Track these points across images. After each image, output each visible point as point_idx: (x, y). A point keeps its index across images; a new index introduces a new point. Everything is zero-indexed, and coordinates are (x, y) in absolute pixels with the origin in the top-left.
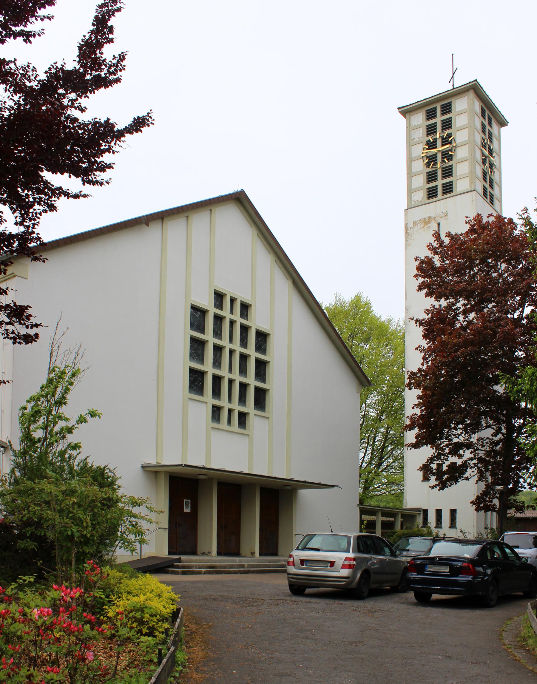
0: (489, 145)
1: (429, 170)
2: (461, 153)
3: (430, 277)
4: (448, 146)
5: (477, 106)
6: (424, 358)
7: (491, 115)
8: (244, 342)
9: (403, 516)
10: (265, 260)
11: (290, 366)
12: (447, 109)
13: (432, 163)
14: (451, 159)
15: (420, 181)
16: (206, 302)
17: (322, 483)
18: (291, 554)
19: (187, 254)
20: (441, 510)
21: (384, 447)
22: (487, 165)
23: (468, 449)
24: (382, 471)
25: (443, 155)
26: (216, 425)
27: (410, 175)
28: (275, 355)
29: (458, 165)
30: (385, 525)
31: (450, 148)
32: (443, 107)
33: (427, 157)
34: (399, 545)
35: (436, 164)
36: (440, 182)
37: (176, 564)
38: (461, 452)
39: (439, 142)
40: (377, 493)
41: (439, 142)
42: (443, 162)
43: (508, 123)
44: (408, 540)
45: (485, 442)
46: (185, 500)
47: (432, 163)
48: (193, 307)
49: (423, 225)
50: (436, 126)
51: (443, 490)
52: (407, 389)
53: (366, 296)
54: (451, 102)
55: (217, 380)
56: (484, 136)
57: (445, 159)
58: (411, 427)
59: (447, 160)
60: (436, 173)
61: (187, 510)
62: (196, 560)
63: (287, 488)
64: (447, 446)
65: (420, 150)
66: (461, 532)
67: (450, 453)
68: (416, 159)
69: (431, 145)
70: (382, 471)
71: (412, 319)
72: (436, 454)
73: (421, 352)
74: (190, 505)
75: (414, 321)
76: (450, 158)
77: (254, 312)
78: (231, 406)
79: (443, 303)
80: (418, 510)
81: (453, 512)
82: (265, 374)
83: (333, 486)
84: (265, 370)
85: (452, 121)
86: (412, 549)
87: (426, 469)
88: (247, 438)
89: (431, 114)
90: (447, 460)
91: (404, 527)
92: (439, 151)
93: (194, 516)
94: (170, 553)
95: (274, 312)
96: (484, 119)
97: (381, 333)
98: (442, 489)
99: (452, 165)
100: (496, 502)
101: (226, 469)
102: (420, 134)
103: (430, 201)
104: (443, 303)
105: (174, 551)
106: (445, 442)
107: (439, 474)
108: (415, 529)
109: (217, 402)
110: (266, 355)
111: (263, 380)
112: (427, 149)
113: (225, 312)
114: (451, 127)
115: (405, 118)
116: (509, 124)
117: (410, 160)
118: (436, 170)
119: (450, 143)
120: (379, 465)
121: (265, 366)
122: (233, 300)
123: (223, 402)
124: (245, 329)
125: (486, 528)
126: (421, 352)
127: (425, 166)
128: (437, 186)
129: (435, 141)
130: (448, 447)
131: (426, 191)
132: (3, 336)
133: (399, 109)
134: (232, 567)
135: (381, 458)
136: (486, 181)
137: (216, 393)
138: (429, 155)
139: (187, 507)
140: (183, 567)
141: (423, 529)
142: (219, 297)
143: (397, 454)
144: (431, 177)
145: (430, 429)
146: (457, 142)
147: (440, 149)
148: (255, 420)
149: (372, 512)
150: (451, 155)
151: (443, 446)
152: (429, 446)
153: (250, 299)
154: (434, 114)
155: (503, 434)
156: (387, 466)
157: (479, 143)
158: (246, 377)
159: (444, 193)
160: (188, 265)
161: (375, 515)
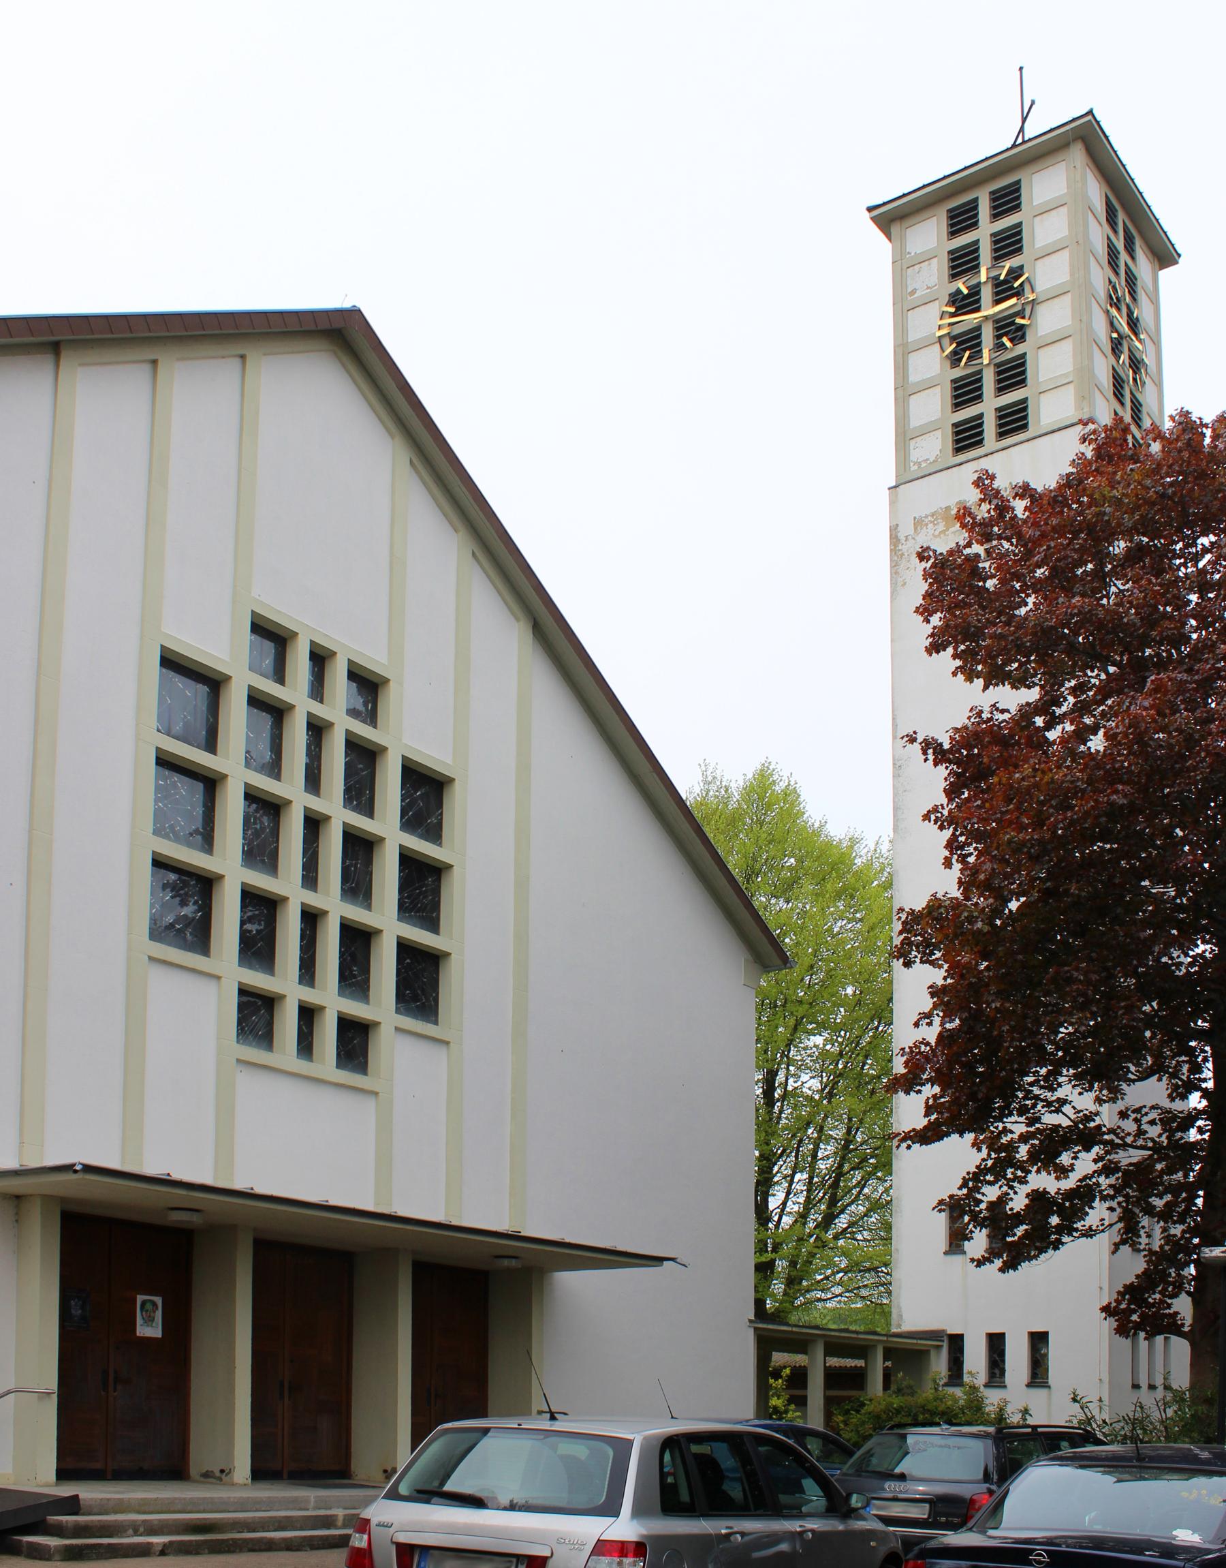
0: (1128, 306)
1: (958, 373)
2: (1049, 320)
3: (964, 608)
4: (1013, 301)
5: (1095, 192)
6: (951, 845)
7: (1134, 232)
8: (360, 793)
9: (889, 1353)
10: (438, 547)
11: (522, 884)
12: (1007, 201)
13: (968, 353)
14: (1022, 338)
15: (934, 406)
16: (224, 647)
17: (621, 1247)
18: (366, 1514)
19: (150, 481)
20: (1001, 1336)
21: (839, 1173)
22: (1124, 358)
23: (1087, 1149)
24: (836, 1237)
25: (998, 329)
26: (254, 1053)
27: (904, 391)
28: (473, 842)
29: (1041, 351)
30: (833, 1378)
31: (1019, 308)
32: (995, 197)
33: (953, 338)
34: (869, 1454)
35: (977, 354)
36: (990, 405)
37: (53, 1519)
38: (1065, 1159)
39: (987, 294)
40: (819, 1295)
41: (987, 294)
42: (1000, 346)
43: (1179, 256)
44: (904, 1437)
45: (1145, 1119)
46: (140, 1298)
47: (968, 353)
48: (172, 662)
49: (941, 527)
50: (977, 250)
51: (1015, 1269)
52: (898, 964)
53: (786, 772)
54: (1018, 182)
55: (260, 906)
56: (1114, 279)
57: (1005, 340)
58: (909, 1083)
59: (1011, 340)
60: (980, 380)
61: (150, 1329)
62: (145, 1501)
63: (506, 1262)
64: (1024, 1138)
65: (932, 321)
66: (1074, 1400)
67: (1033, 1157)
68: (922, 346)
69: (965, 303)
70: (836, 1237)
71: (912, 740)
72: (990, 1163)
73: (941, 828)
74: (159, 1314)
75: (917, 747)
76: (1019, 334)
77: (392, 702)
78: (310, 996)
79: (1012, 699)
80: (935, 1335)
81: (1038, 1340)
82: (436, 906)
83: (659, 1260)
84: (437, 892)
85: (1024, 234)
86: (916, 1472)
87: (959, 1212)
88: (370, 1104)
89: (962, 220)
90: (1023, 1181)
91: (893, 1387)
92: (986, 318)
93: (176, 1350)
94: (63, 1474)
95: (457, 701)
96: (1115, 232)
97: (832, 871)
98: (1011, 1265)
99: (1023, 355)
100: (1183, 1306)
101: (259, 1190)
102: (933, 277)
103: (962, 457)
104: (1012, 699)
105: (98, 1465)
106: (1017, 1126)
107: (998, 1219)
108: (927, 1393)
109: (258, 980)
110: (440, 845)
111: (433, 924)
112: (953, 315)
113: (295, 691)
114: (1020, 249)
115: (888, 236)
116: (1181, 260)
117: (903, 351)
118: (980, 372)
119: (1019, 293)
120: (829, 1219)
121: (439, 880)
122: (320, 658)
123: (284, 981)
124: (363, 757)
125: (1136, 1386)
126: (941, 828)
127: (948, 363)
128: (981, 416)
129: (975, 291)
130: (1026, 1142)
131: (949, 431)
133: (870, 209)
134: (282, 1524)
135: (833, 1202)
136: (1122, 404)
137: (258, 948)
138: (957, 330)
139: (149, 1320)
140: (80, 1531)
141: (951, 1390)
142: (272, 636)
143: (876, 1195)
144: (966, 391)
145: (974, 1080)
146: (1038, 288)
147: (991, 312)
148: (397, 1045)
149: (799, 1344)
150: (1022, 327)
151: (1011, 1141)
152: (970, 1137)
153: (384, 661)
154: (968, 216)
155: (1206, 1094)
156: (851, 1224)
157: (1102, 295)
158: (369, 907)
159: (1001, 435)
160: (153, 522)
161: (804, 1352)
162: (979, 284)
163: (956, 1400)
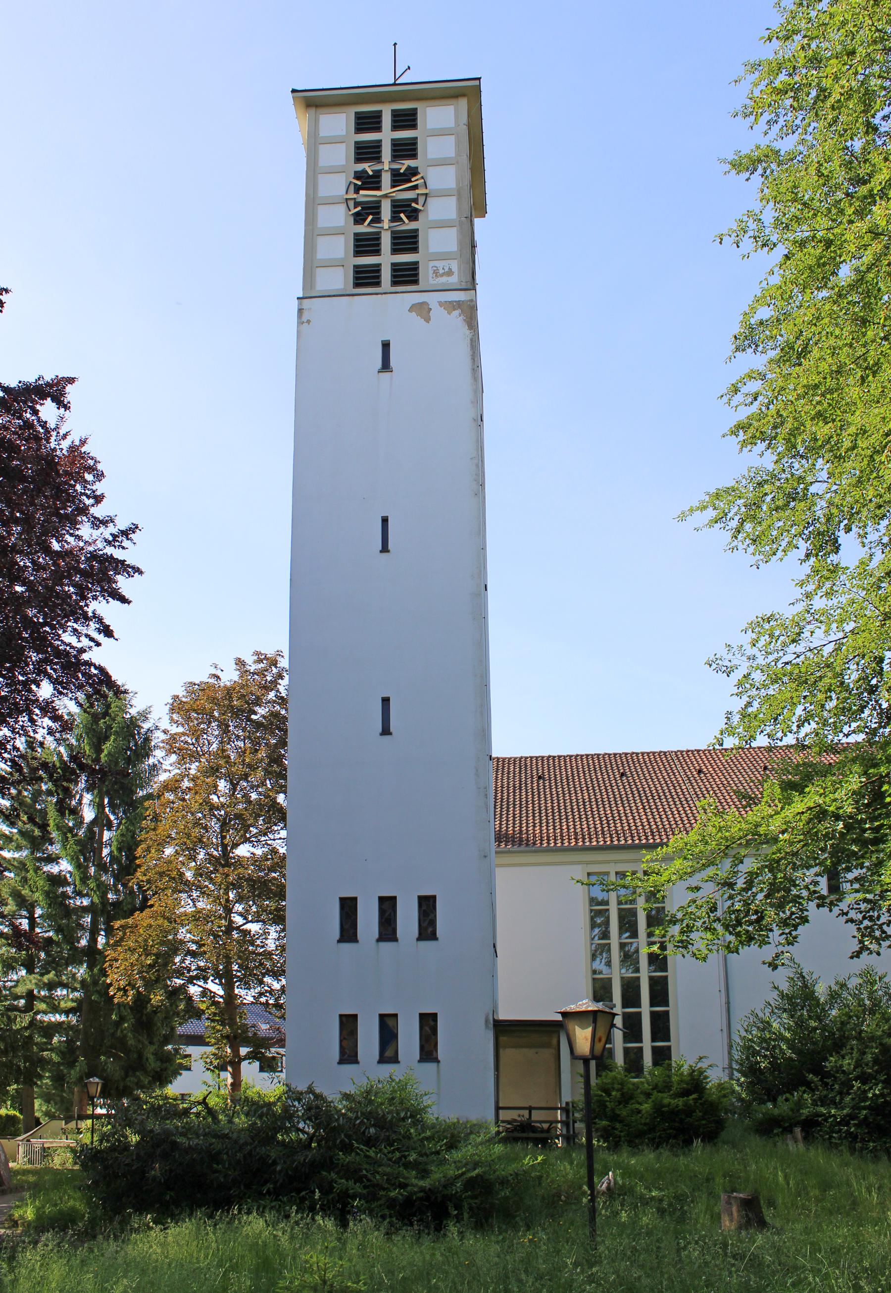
12: (405, 120)
13: (370, 217)
15: (338, 248)
31: (415, 197)
32: (396, 114)
47: (370, 217)
65: (337, 185)
81: (428, 1022)
89: (367, 122)
102: (340, 155)
127: (352, 220)
129: (378, 174)
132: (249, 659)
144: (366, 245)
150: (416, 211)
162: (380, 171)
163: (677, 1106)
